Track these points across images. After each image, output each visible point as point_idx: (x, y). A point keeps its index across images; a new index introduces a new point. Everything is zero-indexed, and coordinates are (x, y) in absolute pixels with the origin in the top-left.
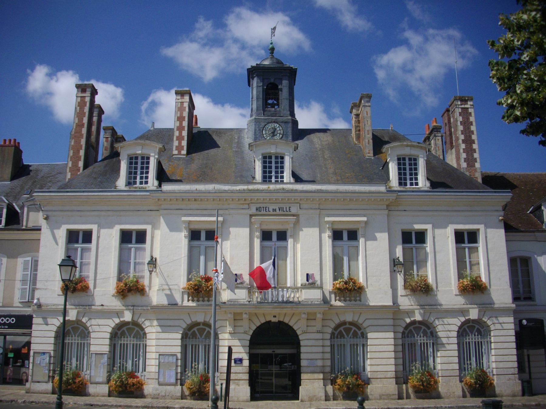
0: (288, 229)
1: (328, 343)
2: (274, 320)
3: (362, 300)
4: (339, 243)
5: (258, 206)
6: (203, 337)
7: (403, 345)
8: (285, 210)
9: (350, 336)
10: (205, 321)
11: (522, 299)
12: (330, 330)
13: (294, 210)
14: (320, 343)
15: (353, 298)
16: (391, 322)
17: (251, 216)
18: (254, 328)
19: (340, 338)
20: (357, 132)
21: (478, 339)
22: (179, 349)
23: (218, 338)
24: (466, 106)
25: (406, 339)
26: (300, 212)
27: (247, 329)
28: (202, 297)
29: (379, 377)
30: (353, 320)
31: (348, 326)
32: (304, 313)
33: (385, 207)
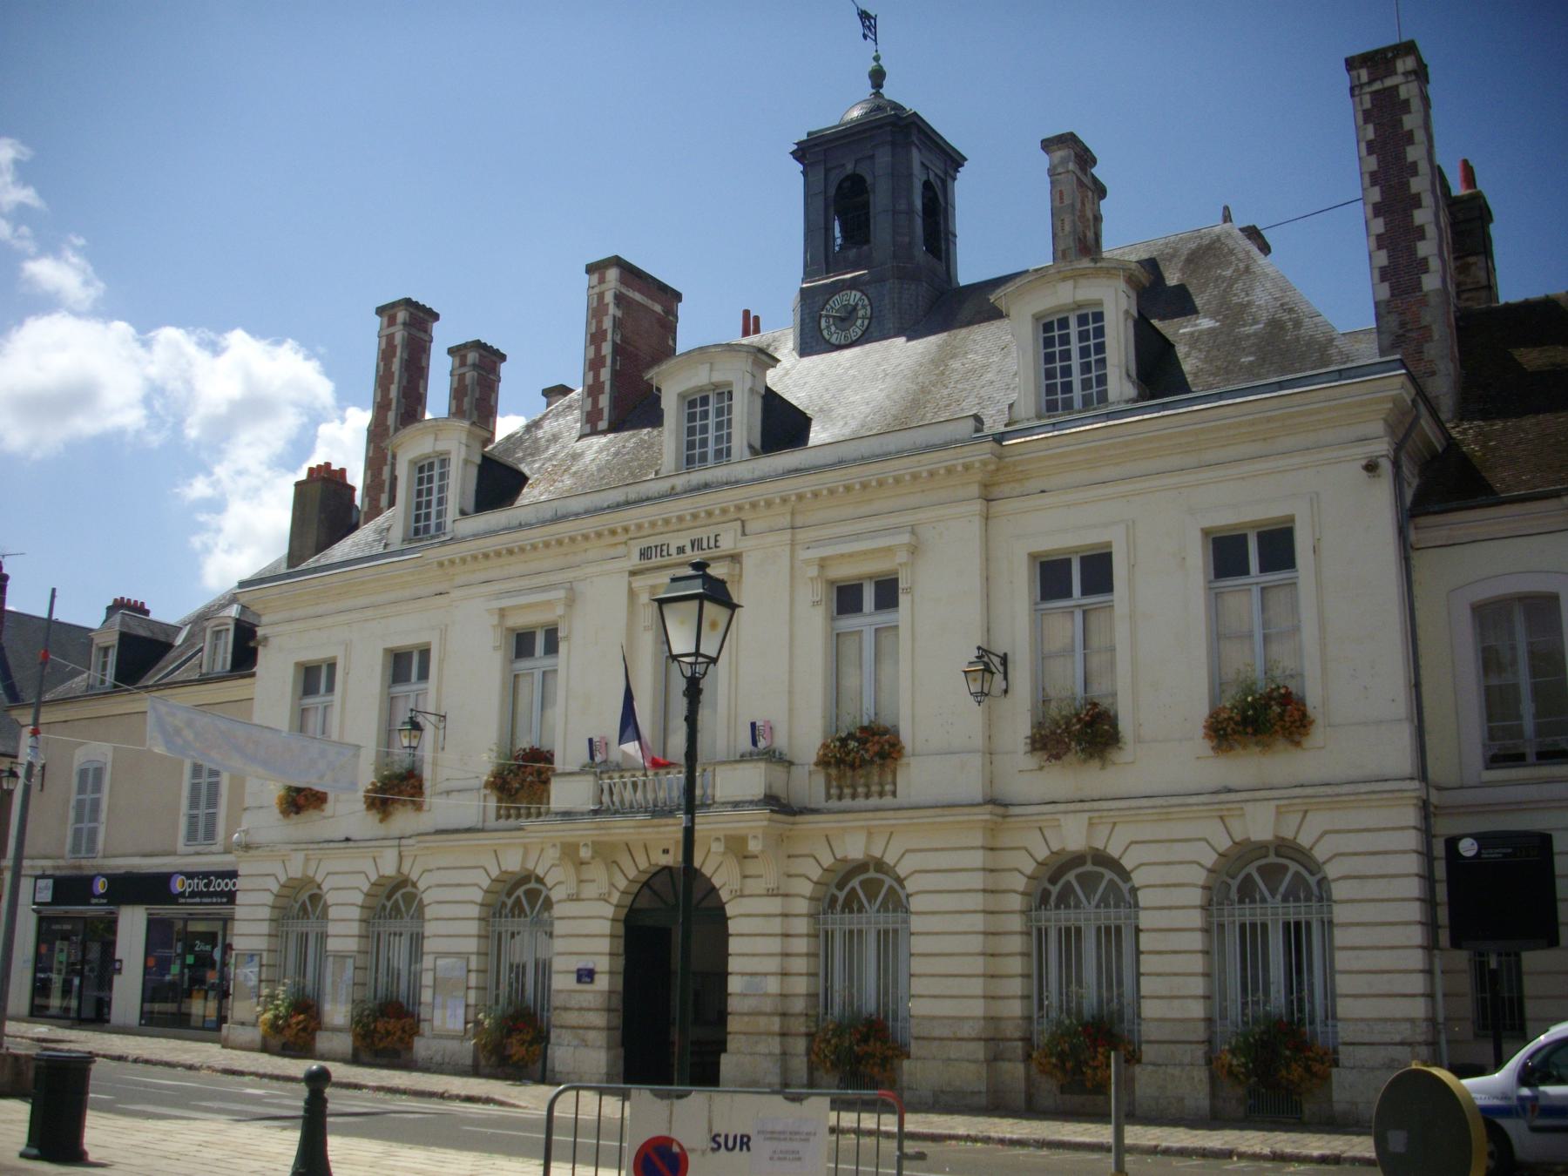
5: (645, 543)
7: (1041, 935)
11: (1531, 758)
14: (776, 926)
16: (977, 859)
18: (622, 884)
19: (895, 910)
21: (888, 920)
23: (1329, 899)
24: (1389, 82)
25: (1052, 914)
26: (744, 545)
32: (718, 839)
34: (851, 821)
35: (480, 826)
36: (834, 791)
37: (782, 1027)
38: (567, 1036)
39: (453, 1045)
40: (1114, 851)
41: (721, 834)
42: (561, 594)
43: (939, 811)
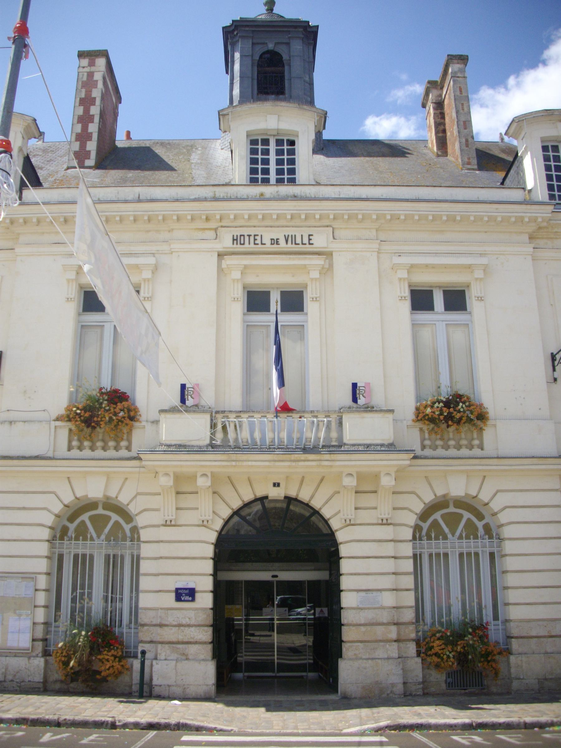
0: (306, 286)
1: (407, 550)
2: (276, 494)
3: (486, 445)
4: (424, 316)
5: (238, 232)
6: (103, 537)
8: (299, 241)
9: (458, 533)
10: (108, 498)
12: (412, 519)
13: (321, 241)
15: (464, 442)
17: (221, 255)
19: (437, 538)
20: (440, 135)
22: (42, 565)
23: (139, 539)
26: (334, 246)
27: (209, 516)
28: (103, 440)
29: (534, 633)
30: (467, 495)
31: (452, 509)
33: (526, 238)
34: (457, 465)
35: (50, 454)
36: (75, 443)
37: (399, 634)
38: (163, 651)
39: (20, 663)
40: (124, 499)
41: (353, 471)
42: (151, 260)
43: (535, 461)
